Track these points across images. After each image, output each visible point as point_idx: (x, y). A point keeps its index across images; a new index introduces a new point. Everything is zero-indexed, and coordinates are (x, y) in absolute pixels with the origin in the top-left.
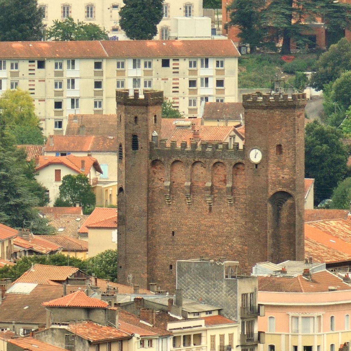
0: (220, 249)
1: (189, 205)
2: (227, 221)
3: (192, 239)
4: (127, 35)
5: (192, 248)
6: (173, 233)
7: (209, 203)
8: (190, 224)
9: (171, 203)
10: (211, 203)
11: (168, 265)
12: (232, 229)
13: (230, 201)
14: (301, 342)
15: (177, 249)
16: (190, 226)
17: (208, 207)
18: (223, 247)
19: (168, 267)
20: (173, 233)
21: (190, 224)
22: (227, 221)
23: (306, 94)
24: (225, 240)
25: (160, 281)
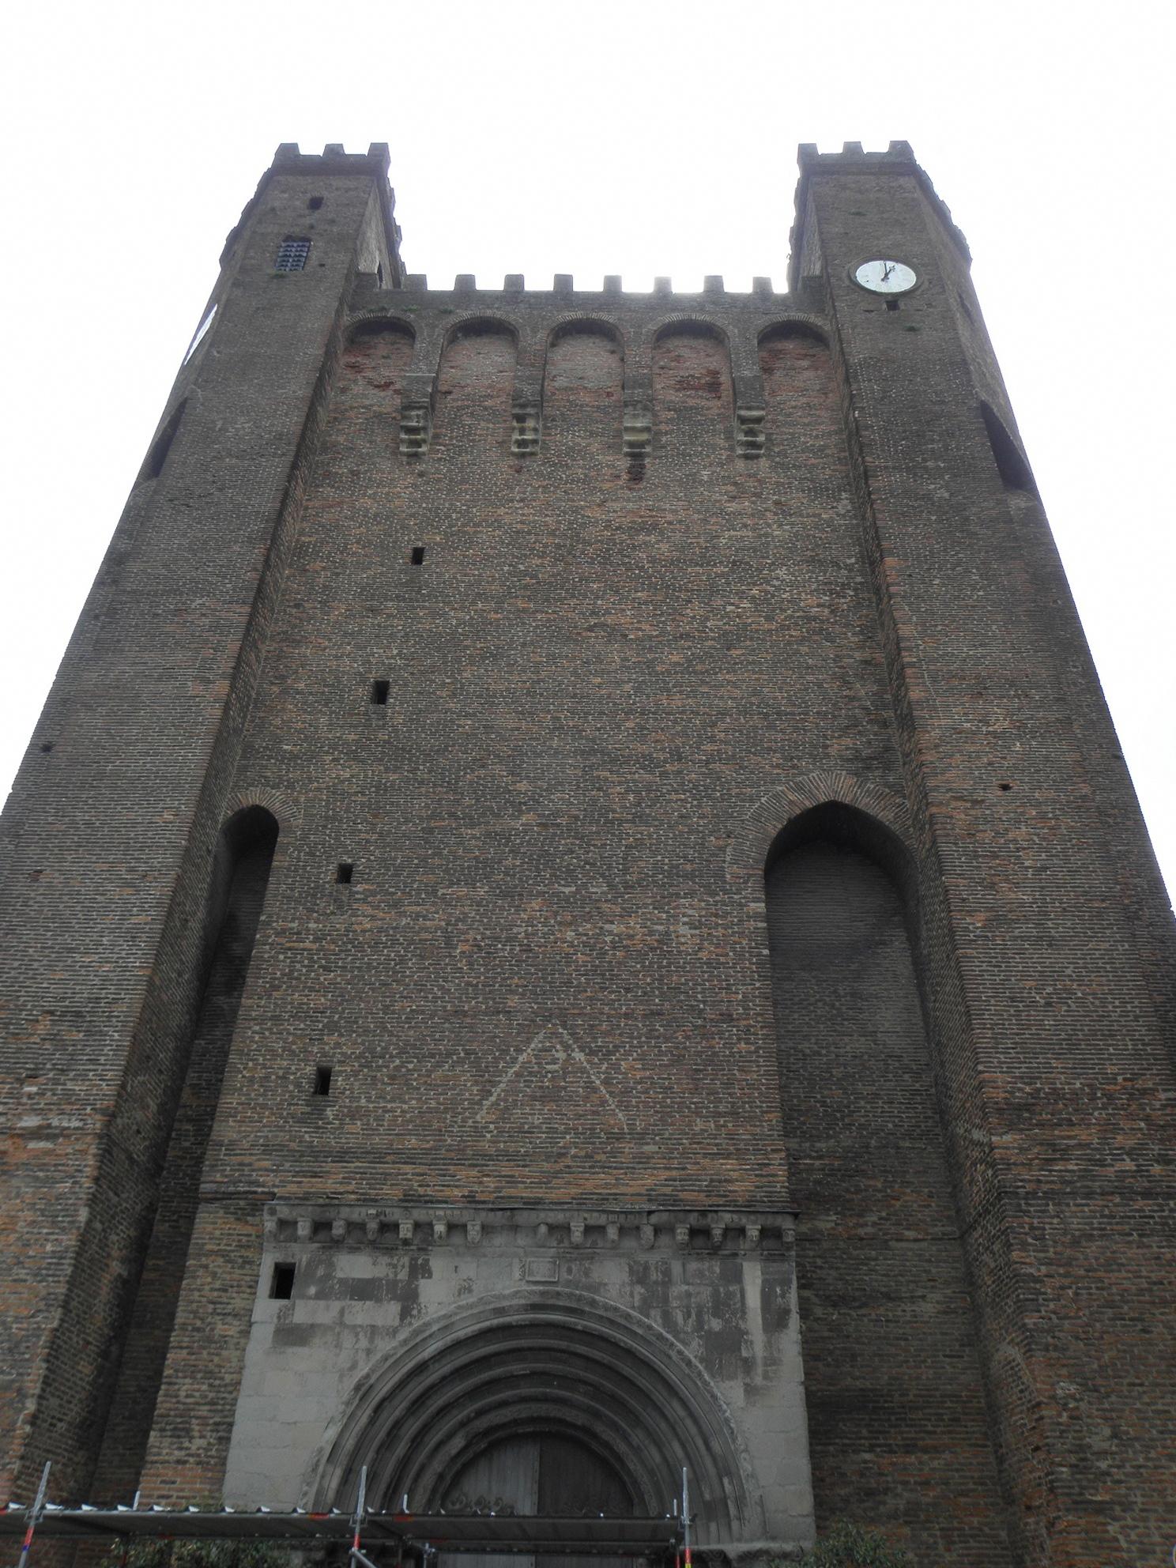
0: (696, 609)
1: (523, 455)
2: (732, 507)
3: (525, 574)
4: (275, 822)
5: (524, 610)
6: (418, 556)
7: (631, 445)
8: (522, 522)
9: (424, 449)
10: (642, 445)
11: (363, 681)
12: (766, 535)
13: (747, 433)
14: (759, 1320)
15: (434, 614)
16: (519, 526)
17: (624, 464)
18: (718, 602)
19: (364, 692)
20: (418, 556)
21: (522, 522)
22: (732, 507)
23: (271, 1296)
24: (722, 575)
25: (295, 757)
